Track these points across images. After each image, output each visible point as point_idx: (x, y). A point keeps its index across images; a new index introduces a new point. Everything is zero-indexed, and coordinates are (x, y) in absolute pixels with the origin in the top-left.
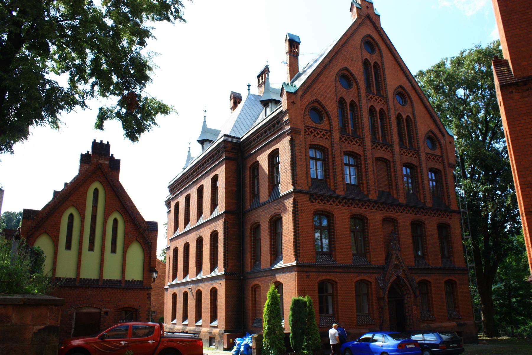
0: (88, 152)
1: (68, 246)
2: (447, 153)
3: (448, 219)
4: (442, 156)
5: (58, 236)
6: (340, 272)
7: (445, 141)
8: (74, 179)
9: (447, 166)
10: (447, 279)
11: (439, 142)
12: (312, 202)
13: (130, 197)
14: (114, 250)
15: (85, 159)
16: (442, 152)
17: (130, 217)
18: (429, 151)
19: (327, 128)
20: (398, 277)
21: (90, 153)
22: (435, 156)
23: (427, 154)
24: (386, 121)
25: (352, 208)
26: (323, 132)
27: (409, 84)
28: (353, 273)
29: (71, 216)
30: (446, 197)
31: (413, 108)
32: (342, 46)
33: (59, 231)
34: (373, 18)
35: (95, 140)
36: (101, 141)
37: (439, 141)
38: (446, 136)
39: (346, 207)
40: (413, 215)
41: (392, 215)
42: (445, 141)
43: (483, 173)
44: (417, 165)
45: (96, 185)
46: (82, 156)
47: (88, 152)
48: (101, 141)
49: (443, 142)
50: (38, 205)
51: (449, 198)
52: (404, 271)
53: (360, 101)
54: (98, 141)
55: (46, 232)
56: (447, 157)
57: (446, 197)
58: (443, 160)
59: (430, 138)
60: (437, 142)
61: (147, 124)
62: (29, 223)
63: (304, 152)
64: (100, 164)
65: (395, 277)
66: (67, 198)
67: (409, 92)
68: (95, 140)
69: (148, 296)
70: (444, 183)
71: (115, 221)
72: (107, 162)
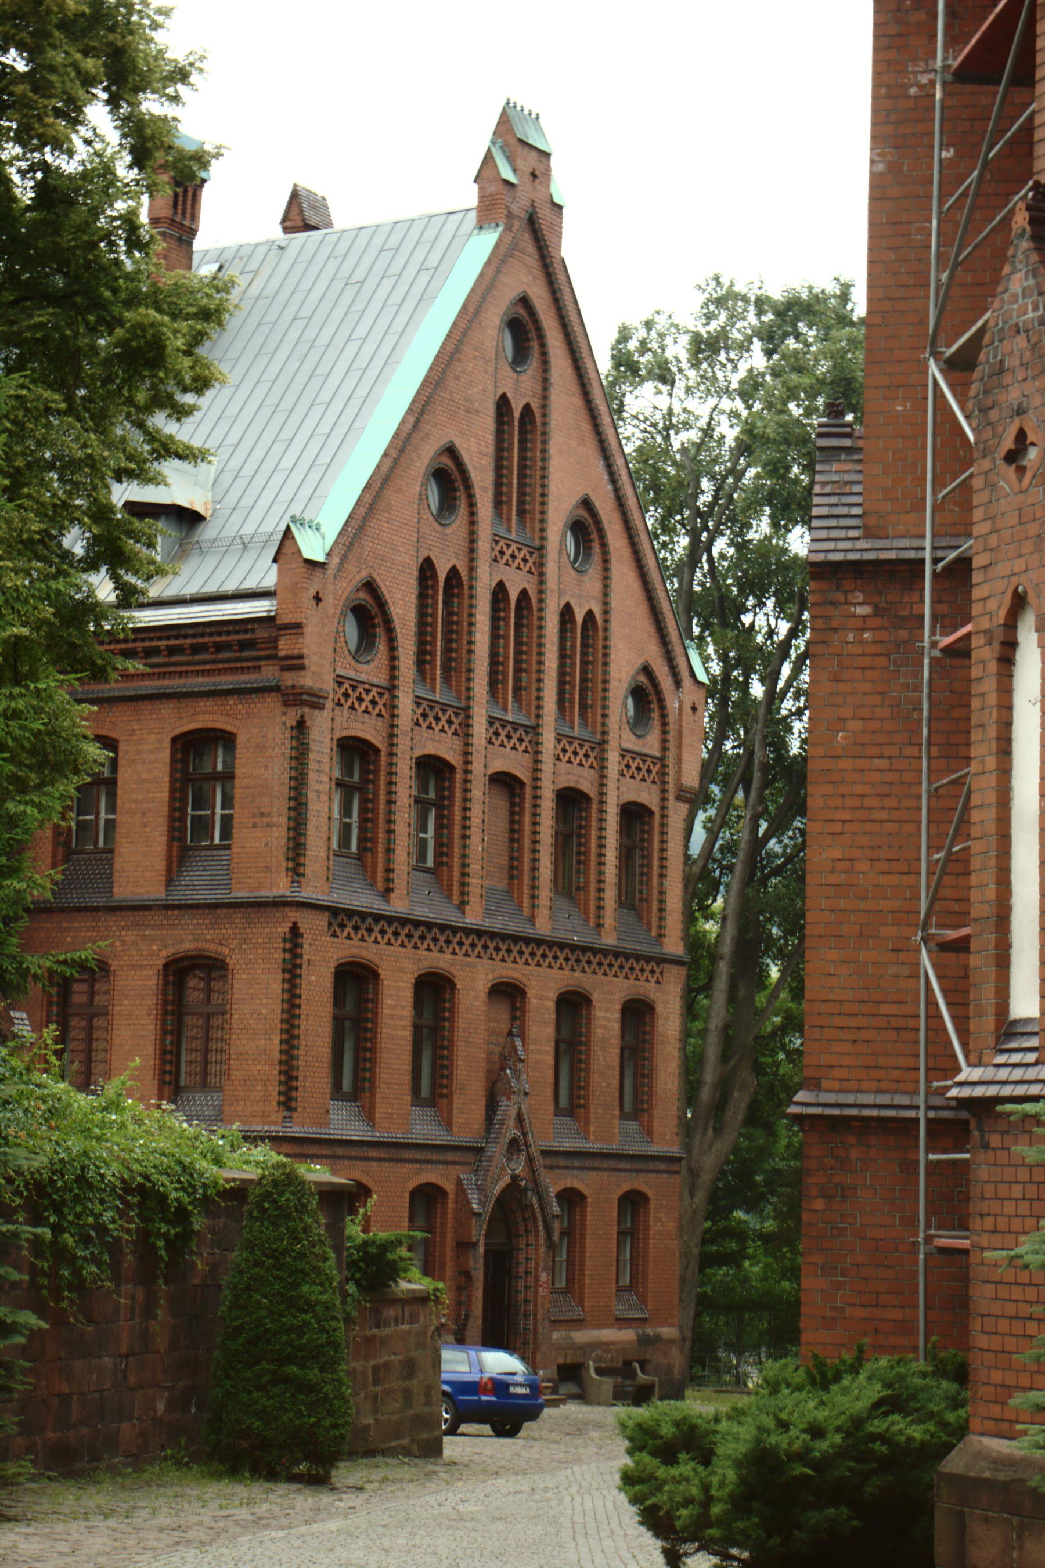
2: (679, 746)
3: (653, 984)
4: (662, 759)
6: (380, 1160)
7: (681, 702)
8: (876, 138)
9: (671, 796)
10: (626, 1187)
11: (662, 707)
12: (334, 935)
16: (664, 749)
18: (630, 742)
19: (380, 678)
20: (515, 1178)
22: (644, 757)
23: (624, 752)
24: (529, 637)
25: (422, 952)
26: (374, 690)
27: (610, 487)
28: (410, 1161)
30: (655, 906)
31: (606, 578)
32: (460, 343)
34: (544, 213)
37: (661, 701)
38: (687, 682)
39: (410, 949)
40: (567, 972)
41: (515, 975)
42: (681, 702)
43: (119, 516)
44: (592, 792)
49: (672, 705)
51: (661, 910)
52: (530, 1159)
53: (472, 569)
56: (679, 761)
57: (655, 906)
58: (663, 773)
59: (359, 611)
60: (655, 706)
63: (327, 770)
65: (507, 1179)
67: (606, 526)
70: (656, 855)
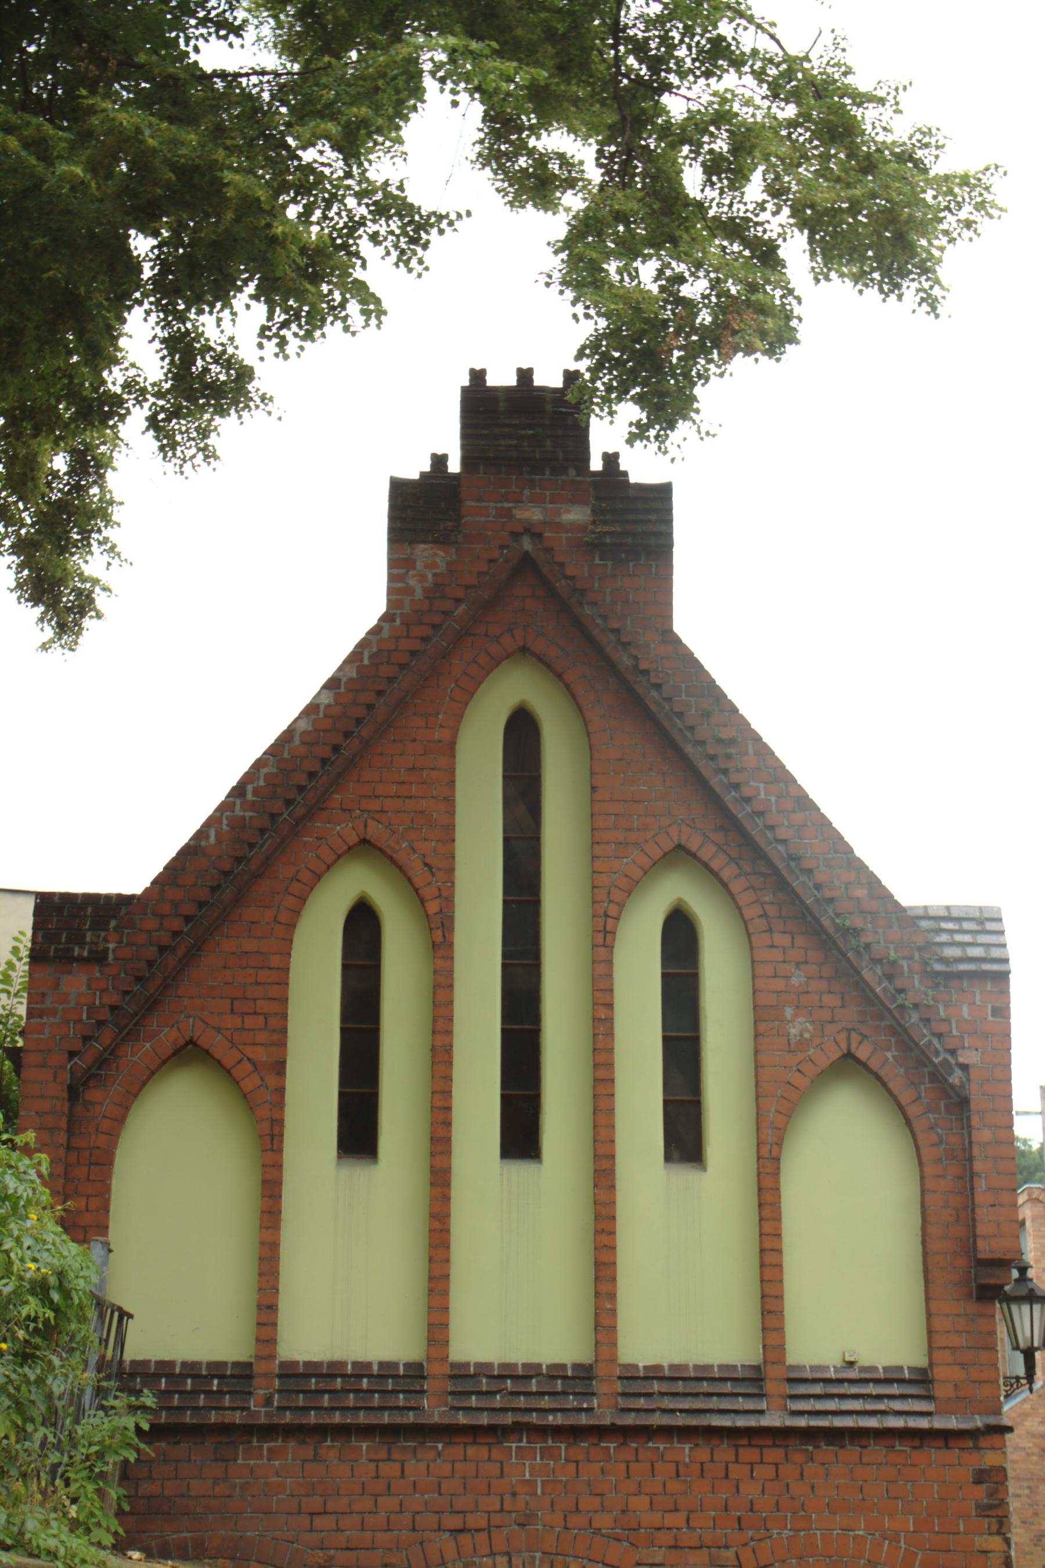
0: (439, 461)
1: (358, 1136)
5: (279, 1067)
8: (238, 791)
13: (769, 738)
14: (684, 1140)
15: (420, 510)
17: (782, 885)
21: (454, 466)
29: (362, 926)
33: (284, 1031)
35: (478, 376)
36: (525, 375)
45: (511, 688)
46: (399, 489)
47: (439, 461)
48: (525, 375)
50: (126, 862)
54: (501, 377)
55: (189, 1053)
61: (26, 572)
62: (77, 984)
64: (534, 532)
66: (329, 784)
68: (478, 376)
69: (980, 1493)
71: (680, 936)
72: (576, 515)
